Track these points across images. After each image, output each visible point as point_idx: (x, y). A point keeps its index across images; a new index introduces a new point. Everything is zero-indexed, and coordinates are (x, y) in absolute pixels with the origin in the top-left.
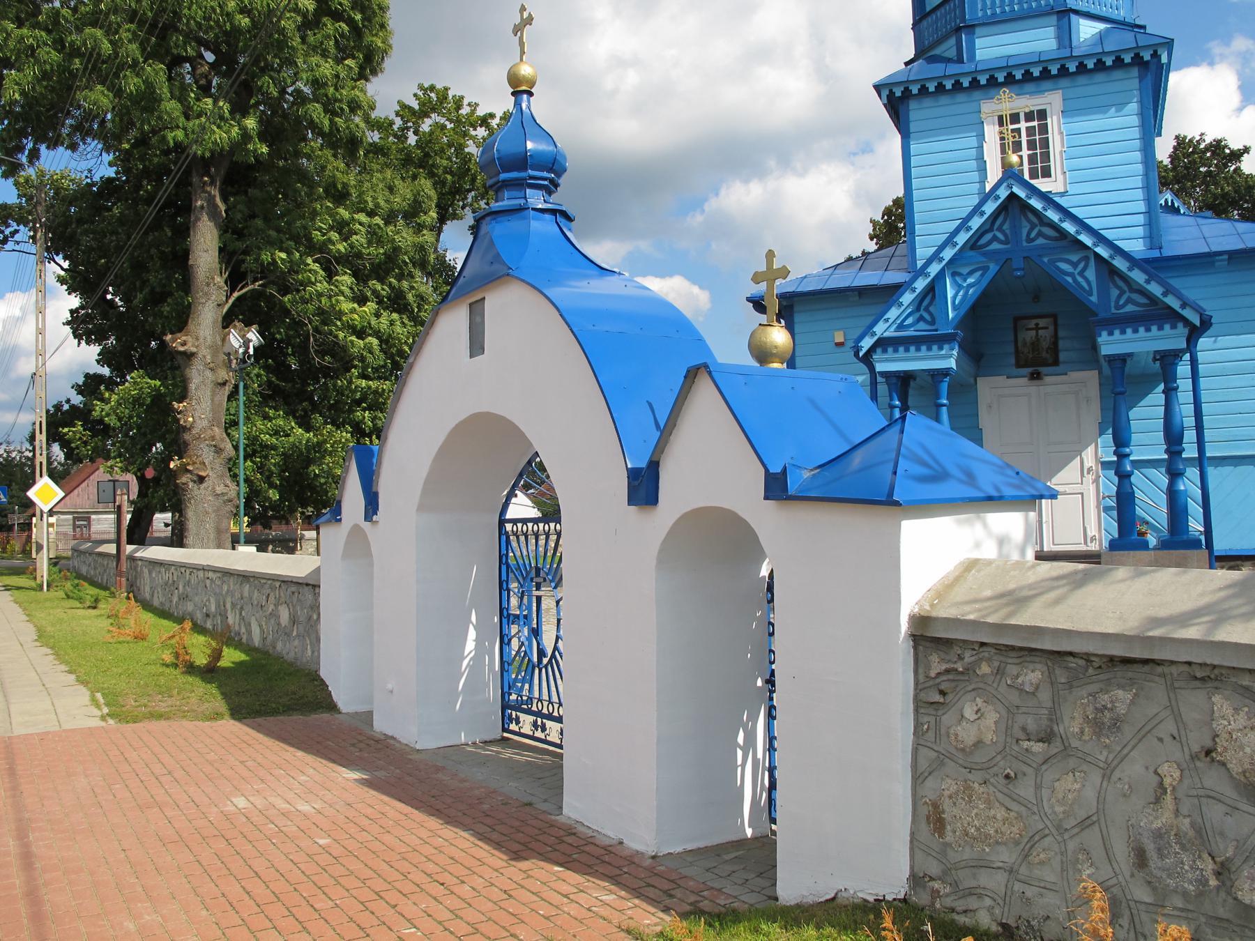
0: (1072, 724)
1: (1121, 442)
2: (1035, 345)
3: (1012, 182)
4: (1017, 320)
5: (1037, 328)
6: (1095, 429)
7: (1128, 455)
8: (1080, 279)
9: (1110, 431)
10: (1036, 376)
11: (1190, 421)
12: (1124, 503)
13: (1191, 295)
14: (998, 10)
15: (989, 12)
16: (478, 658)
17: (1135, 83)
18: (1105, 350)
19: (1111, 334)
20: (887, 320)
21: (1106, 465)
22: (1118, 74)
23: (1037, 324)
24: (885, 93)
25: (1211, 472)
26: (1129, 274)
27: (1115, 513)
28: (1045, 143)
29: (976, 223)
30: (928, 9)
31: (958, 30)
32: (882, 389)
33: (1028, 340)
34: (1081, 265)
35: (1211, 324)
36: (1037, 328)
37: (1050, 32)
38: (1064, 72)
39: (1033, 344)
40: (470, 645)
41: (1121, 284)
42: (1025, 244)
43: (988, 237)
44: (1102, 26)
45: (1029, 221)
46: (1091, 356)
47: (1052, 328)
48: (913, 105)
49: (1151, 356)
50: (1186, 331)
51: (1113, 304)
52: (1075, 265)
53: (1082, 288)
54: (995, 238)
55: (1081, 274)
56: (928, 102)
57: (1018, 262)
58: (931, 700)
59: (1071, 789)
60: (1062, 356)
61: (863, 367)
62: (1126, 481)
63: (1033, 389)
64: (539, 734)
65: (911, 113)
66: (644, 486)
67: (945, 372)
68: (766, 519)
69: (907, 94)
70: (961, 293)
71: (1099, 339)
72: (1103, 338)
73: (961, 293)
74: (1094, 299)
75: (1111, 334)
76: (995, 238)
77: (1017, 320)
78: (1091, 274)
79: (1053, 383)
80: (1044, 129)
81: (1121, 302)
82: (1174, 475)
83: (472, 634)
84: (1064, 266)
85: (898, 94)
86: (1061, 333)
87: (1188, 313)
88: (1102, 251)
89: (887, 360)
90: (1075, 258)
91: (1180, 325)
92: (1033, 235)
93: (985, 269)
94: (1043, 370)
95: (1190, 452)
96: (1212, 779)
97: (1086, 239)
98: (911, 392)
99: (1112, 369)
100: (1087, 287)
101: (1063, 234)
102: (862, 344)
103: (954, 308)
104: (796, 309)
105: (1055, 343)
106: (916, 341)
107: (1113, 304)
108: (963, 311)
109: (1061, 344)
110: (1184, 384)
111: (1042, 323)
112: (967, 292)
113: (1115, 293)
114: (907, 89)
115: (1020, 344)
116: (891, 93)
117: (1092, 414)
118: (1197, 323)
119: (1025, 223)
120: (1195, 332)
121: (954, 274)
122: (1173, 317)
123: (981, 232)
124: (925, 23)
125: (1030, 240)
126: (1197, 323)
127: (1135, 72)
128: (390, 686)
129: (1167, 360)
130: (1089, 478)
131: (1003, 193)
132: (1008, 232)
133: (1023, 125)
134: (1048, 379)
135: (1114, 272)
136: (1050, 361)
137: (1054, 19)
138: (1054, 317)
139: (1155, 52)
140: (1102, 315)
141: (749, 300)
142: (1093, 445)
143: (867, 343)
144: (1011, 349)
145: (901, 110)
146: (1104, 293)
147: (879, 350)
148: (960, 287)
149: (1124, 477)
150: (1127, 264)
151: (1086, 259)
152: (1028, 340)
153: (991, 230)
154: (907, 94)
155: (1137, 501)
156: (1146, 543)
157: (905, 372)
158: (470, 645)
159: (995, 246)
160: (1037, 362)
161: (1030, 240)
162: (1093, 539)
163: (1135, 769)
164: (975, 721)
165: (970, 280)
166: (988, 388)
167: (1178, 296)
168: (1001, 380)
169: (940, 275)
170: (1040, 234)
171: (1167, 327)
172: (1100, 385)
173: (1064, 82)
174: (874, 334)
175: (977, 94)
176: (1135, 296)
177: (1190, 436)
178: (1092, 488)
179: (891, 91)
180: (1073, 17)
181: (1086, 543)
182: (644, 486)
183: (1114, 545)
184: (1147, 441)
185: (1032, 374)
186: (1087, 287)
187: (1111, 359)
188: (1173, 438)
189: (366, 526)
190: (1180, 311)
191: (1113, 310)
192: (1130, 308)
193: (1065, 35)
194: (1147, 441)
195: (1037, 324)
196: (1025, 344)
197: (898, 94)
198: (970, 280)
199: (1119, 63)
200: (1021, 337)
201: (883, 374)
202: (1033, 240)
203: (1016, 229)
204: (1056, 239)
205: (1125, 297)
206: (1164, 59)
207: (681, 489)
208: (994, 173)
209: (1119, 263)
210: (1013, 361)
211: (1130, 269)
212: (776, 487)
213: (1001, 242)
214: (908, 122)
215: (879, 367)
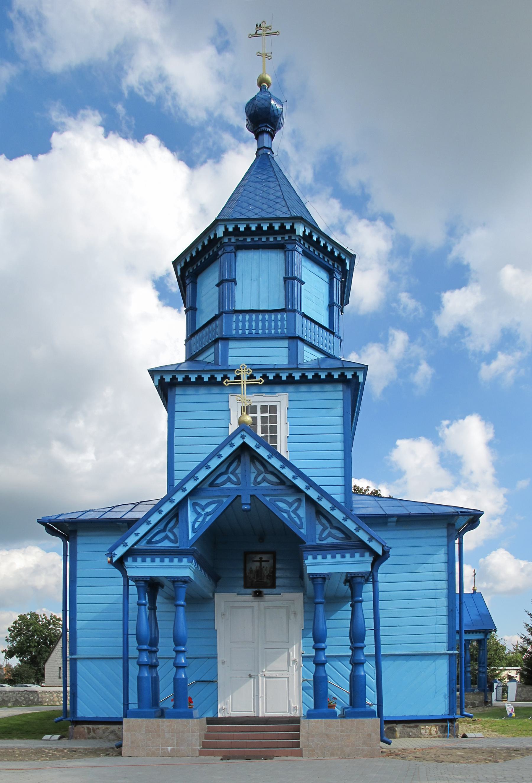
1: (319, 639)
2: (259, 572)
3: (245, 434)
5: (261, 561)
6: (299, 633)
7: (323, 649)
8: (293, 516)
9: (311, 634)
10: (258, 595)
11: (370, 623)
12: (319, 686)
14: (247, 332)
15: (240, 332)
17: (340, 395)
18: (311, 570)
19: (315, 558)
20: (137, 534)
21: (305, 658)
22: (328, 387)
23: (261, 558)
25: (384, 664)
26: (331, 512)
27: (312, 692)
29: (214, 463)
30: (197, 328)
31: (216, 341)
32: (133, 589)
33: (254, 568)
34: (296, 505)
35: (389, 556)
36: (261, 561)
37: (285, 352)
38: (290, 380)
39: (257, 571)
41: (324, 521)
42: (252, 485)
44: (320, 356)
45: (256, 468)
46: (299, 579)
47: (271, 561)
49: (344, 578)
50: (371, 559)
51: (317, 536)
52: (290, 505)
53: (295, 523)
54: (229, 480)
55: (295, 511)
56: (191, 390)
57: (246, 499)
60: (278, 582)
62: (321, 668)
63: (255, 603)
65: (177, 397)
67: (185, 581)
69: (174, 383)
70: (200, 519)
71: (306, 561)
72: (309, 560)
73: (200, 519)
74: (303, 531)
75: (315, 558)
76: (229, 480)
78: (302, 512)
79: (270, 599)
80: (274, 419)
81: (324, 536)
82: (356, 664)
84: (281, 505)
85: (168, 379)
86: (278, 566)
87: (374, 545)
88: (313, 494)
89: (136, 567)
90: (290, 499)
91: (367, 554)
92: (259, 479)
94: (265, 591)
95: (369, 650)
97: (301, 484)
98: (159, 599)
99: (314, 585)
100: (299, 523)
102: (116, 552)
104: (79, 534)
106: (163, 553)
107: (317, 536)
108: (200, 533)
109: (278, 574)
110: (367, 606)
111: (265, 557)
112: (204, 519)
114: (174, 378)
115: (248, 571)
116: (162, 380)
117: (297, 623)
118: (380, 553)
119: (253, 470)
120: (378, 559)
121: (194, 505)
124: (194, 340)
125: (257, 483)
126: (380, 553)
127: (340, 387)
129: (353, 581)
130: (294, 667)
131: (238, 442)
132: (239, 475)
133: (259, 415)
134: (267, 597)
135: (320, 512)
136: (269, 585)
137: (286, 343)
138: (274, 554)
139: (355, 373)
140: (308, 543)
141: (39, 521)
142: (298, 644)
143: (120, 551)
144: (242, 575)
145: (170, 394)
146: (311, 528)
147: (130, 559)
149: (319, 664)
150: (330, 505)
151: (300, 500)
152: (254, 568)
155: (329, 685)
156: (335, 713)
157: (151, 578)
159: (229, 485)
160: (259, 584)
161: (257, 483)
162: (295, 708)
165: (209, 509)
166: (222, 601)
168: (232, 596)
169: (184, 501)
170: (264, 480)
171: (357, 555)
172: (304, 603)
173: (291, 388)
174: (126, 545)
176: (335, 532)
177: (369, 639)
178: (295, 674)
179: (162, 377)
180: (300, 344)
181: (289, 711)
183: (310, 715)
184: (338, 644)
185: (255, 592)
186: (299, 523)
187: (314, 578)
188: (356, 638)
190: (368, 542)
191: (318, 542)
192: (330, 540)
193: (293, 354)
194: (338, 644)
195: (261, 558)
196: (251, 571)
198: (209, 509)
199: (330, 379)
200: (249, 566)
202: (259, 483)
204: (278, 484)
205: (326, 532)
206: (361, 380)
208: (234, 427)
209: (325, 504)
210: (242, 583)
211: (332, 509)
213: (233, 482)
214: (174, 403)
215: (131, 572)
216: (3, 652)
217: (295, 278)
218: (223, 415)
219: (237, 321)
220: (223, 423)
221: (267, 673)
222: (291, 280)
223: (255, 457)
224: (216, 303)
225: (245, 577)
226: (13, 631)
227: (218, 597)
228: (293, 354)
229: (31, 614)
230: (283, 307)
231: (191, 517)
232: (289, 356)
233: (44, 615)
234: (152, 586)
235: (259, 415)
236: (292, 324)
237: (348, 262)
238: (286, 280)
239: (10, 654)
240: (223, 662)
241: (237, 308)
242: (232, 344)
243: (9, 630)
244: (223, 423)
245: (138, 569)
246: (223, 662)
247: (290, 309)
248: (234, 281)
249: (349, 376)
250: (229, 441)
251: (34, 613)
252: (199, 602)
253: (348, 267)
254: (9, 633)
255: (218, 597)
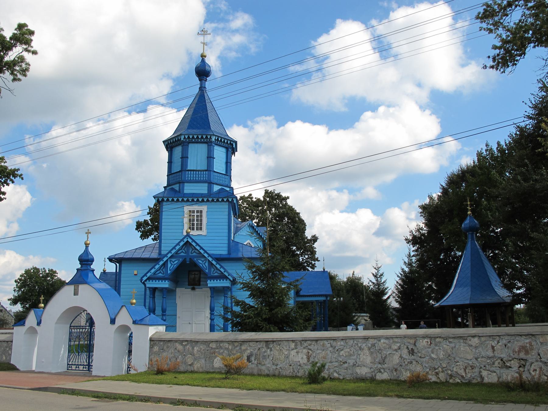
0: (165, 348)
4: (189, 271)
10: (193, 289)
13: (230, 271)
16: (63, 355)
24: (157, 199)
28: (201, 220)
29: (178, 248)
32: (148, 292)
37: (206, 188)
40: (62, 352)
43: (181, 251)
48: (164, 203)
52: (203, 261)
54: (182, 252)
55: (204, 264)
57: (188, 260)
58: (151, 347)
59: (165, 354)
60: (202, 283)
61: (143, 285)
64: (77, 369)
66: (113, 321)
68: (133, 328)
72: (209, 282)
74: (207, 271)
76: (182, 252)
77: (189, 271)
78: (207, 264)
80: (201, 216)
83: (63, 349)
84: (200, 261)
85: (160, 200)
87: (229, 277)
90: (203, 259)
93: (179, 260)
94: (196, 287)
96: (176, 351)
101: (201, 253)
103: (170, 270)
105: (200, 279)
106: (159, 279)
108: (173, 270)
109: (201, 279)
111: (196, 273)
113: (213, 270)
121: (170, 261)
122: (226, 278)
123: (179, 250)
124: (171, 176)
127: (227, 203)
128: (43, 360)
131: (185, 240)
133: (196, 214)
134: (197, 290)
137: (206, 185)
146: (210, 270)
148: (172, 264)
153: (181, 249)
154: (163, 200)
158: (62, 352)
159: (182, 254)
163: (170, 351)
164: (156, 349)
166: (179, 291)
167: (228, 272)
168: (183, 289)
169: (167, 260)
170: (194, 252)
173: (208, 203)
175: (183, 203)
182: (113, 321)
189: (37, 327)
192: (216, 274)
197: (160, 200)
201: (148, 287)
203: (188, 250)
207: (120, 321)
212: (134, 322)
216: (9, 300)
217: (211, 157)
218: (181, 227)
219: (188, 174)
220: (180, 231)
221: (196, 322)
222: (210, 158)
223: (191, 244)
224: (181, 154)
225: (189, 281)
226: (19, 283)
227: (177, 289)
228: (210, 189)
229: (34, 268)
230: (206, 169)
231: (169, 265)
232: (208, 190)
233: (44, 268)
234: (154, 290)
235: (196, 214)
236: (209, 176)
237: (234, 144)
238: (208, 157)
239: (14, 301)
240: (179, 317)
241: (189, 168)
242: (186, 184)
243: (16, 281)
244: (181, 227)
245: (151, 284)
246: (179, 317)
247: (209, 168)
248: (188, 157)
249: (230, 200)
250: (182, 240)
251: (36, 268)
252: (169, 293)
253: (234, 146)
254: (15, 284)
255: (177, 289)
